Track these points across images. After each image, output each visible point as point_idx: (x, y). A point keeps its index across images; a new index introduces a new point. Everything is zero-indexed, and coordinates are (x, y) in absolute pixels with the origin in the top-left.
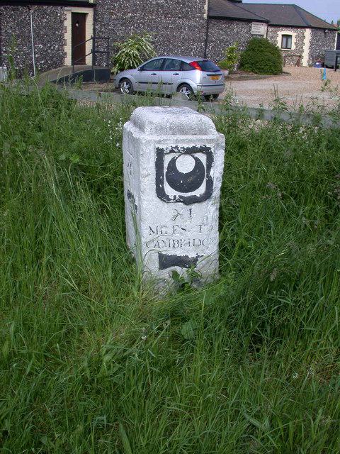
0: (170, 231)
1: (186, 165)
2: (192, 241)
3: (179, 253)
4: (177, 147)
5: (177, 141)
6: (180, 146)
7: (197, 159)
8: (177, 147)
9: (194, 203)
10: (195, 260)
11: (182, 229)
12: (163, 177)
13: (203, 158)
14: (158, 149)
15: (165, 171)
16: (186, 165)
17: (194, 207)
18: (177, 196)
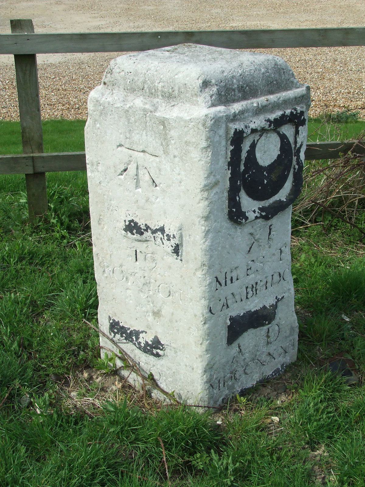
3: (254, 305)
10: (275, 307)
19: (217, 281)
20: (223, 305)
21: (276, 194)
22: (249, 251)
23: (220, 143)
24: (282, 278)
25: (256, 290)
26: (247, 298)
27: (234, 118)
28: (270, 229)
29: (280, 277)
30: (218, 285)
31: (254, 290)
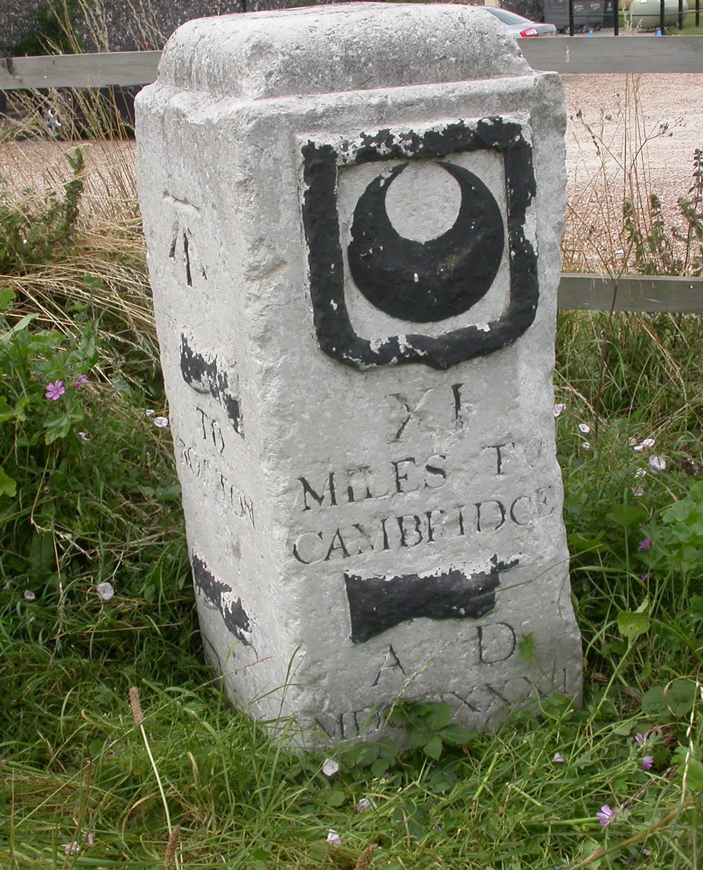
0: (381, 481)
1: (424, 208)
2: (469, 513)
3: (428, 564)
4: (384, 136)
5: (383, 112)
6: (396, 129)
7: (466, 180)
8: (384, 136)
9: (470, 357)
10: (490, 582)
11: (430, 469)
12: (340, 265)
13: (489, 171)
14: (309, 150)
15: (346, 239)
16: (424, 208)
17: (472, 376)
18: (403, 342)
19: (307, 487)
20: (332, 548)
21: (462, 311)
22: (398, 436)
23: (277, 175)
24: (507, 516)
25: (431, 531)
26: (403, 543)
27: (311, 121)
28: (457, 396)
29: (503, 512)
30: (311, 501)
31: (422, 528)
